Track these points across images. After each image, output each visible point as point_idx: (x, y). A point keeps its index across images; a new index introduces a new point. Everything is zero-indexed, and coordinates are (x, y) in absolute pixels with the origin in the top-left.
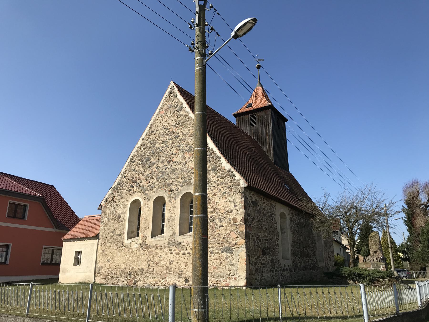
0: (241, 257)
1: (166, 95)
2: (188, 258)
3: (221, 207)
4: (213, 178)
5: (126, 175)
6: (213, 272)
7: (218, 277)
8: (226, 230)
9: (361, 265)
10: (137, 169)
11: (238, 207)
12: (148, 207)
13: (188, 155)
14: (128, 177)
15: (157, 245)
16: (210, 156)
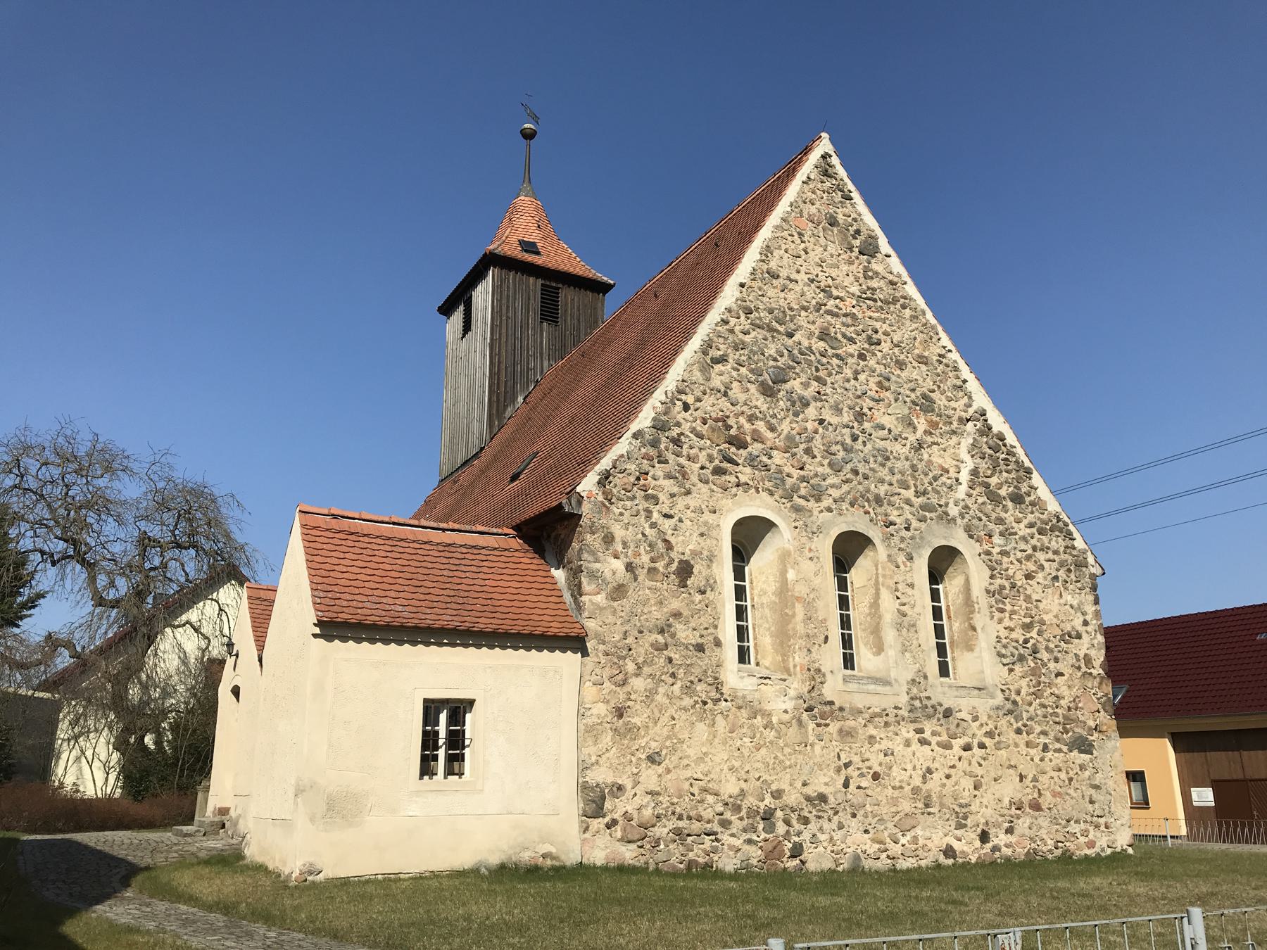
5: (690, 399)
7: (1068, 821)
15: (869, 708)
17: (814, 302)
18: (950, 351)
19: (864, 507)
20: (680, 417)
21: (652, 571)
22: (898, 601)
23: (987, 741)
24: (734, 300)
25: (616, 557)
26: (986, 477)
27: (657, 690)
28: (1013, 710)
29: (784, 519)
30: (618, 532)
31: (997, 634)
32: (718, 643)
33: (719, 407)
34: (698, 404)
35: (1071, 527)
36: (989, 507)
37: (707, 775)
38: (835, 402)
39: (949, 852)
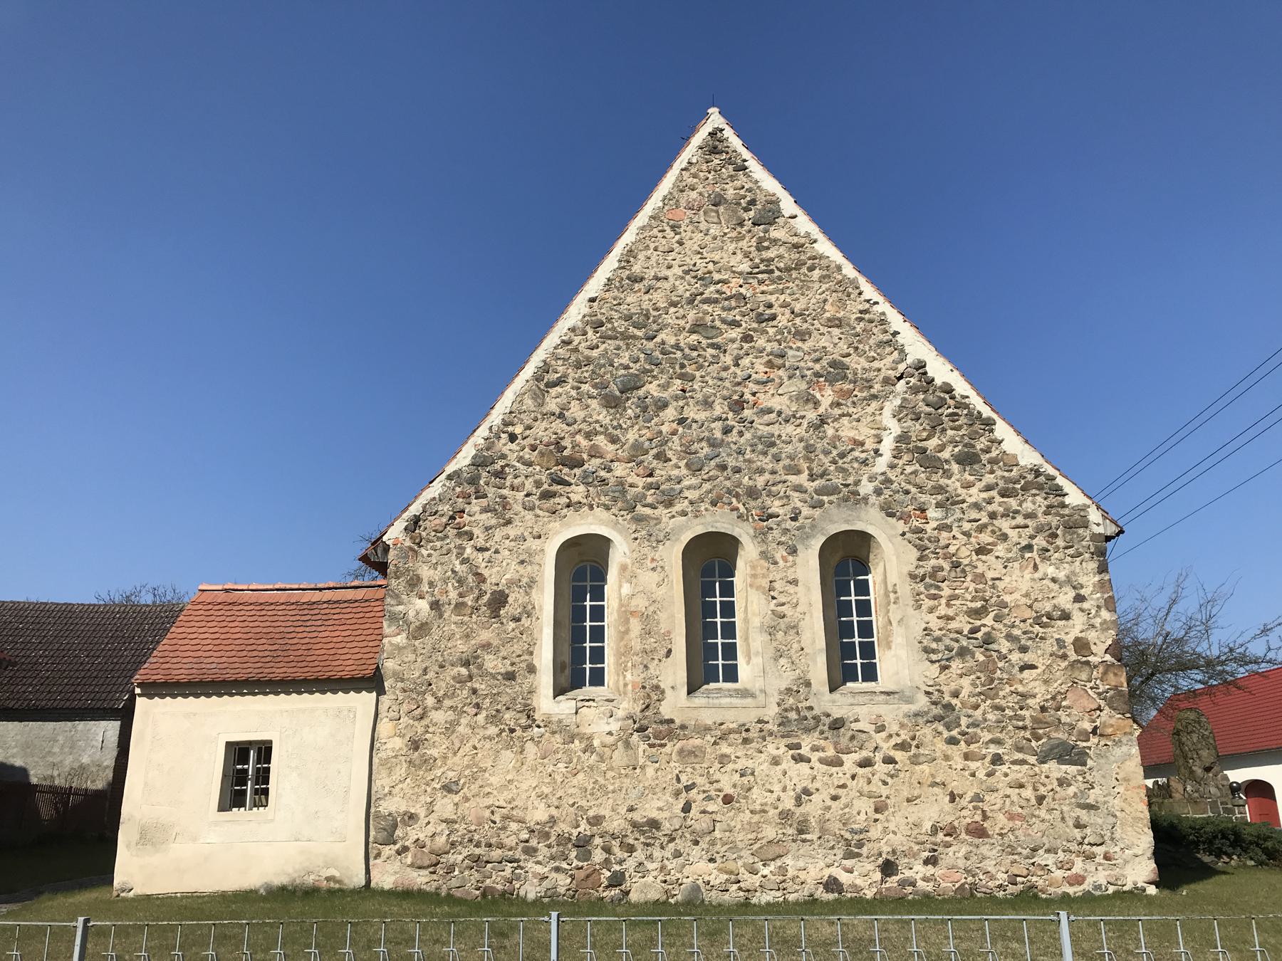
0: (1127, 780)
1: (690, 152)
2: (889, 780)
3: (1017, 596)
4: (965, 491)
5: (518, 430)
6: (1010, 834)
7: (1034, 850)
8: (1046, 682)
9: (1180, 806)
10: (575, 411)
11: (1092, 602)
12: (659, 569)
13: (828, 391)
14: (530, 441)
15: (722, 724)
16: (940, 411)
17: (688, 294)
18: (876, 303)
19: (730, 504)
20: (505, 450)
21: (459, 607)
22: (775, 601)
23: (898, 755)
24: (580, 317)
25: (421, 597)
26: (921, 441)
27: (458, 722)
28: (944, 713)
29: (620, 532)
30: (426, 572)
31: (924, 626)
32: (532, 669)
33: (552, 430)
34: (528, 432)
35: (1060, 481)
36: (922, 475)
37: (510, 803)
38: (703, 396)
39: (832, 884)
